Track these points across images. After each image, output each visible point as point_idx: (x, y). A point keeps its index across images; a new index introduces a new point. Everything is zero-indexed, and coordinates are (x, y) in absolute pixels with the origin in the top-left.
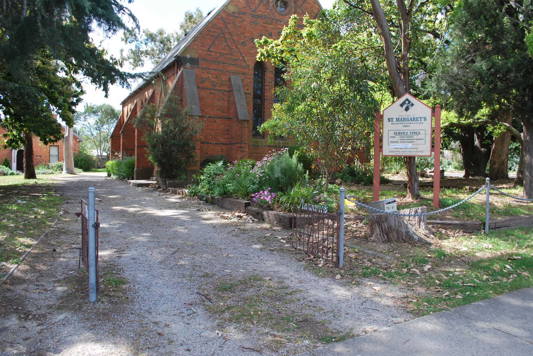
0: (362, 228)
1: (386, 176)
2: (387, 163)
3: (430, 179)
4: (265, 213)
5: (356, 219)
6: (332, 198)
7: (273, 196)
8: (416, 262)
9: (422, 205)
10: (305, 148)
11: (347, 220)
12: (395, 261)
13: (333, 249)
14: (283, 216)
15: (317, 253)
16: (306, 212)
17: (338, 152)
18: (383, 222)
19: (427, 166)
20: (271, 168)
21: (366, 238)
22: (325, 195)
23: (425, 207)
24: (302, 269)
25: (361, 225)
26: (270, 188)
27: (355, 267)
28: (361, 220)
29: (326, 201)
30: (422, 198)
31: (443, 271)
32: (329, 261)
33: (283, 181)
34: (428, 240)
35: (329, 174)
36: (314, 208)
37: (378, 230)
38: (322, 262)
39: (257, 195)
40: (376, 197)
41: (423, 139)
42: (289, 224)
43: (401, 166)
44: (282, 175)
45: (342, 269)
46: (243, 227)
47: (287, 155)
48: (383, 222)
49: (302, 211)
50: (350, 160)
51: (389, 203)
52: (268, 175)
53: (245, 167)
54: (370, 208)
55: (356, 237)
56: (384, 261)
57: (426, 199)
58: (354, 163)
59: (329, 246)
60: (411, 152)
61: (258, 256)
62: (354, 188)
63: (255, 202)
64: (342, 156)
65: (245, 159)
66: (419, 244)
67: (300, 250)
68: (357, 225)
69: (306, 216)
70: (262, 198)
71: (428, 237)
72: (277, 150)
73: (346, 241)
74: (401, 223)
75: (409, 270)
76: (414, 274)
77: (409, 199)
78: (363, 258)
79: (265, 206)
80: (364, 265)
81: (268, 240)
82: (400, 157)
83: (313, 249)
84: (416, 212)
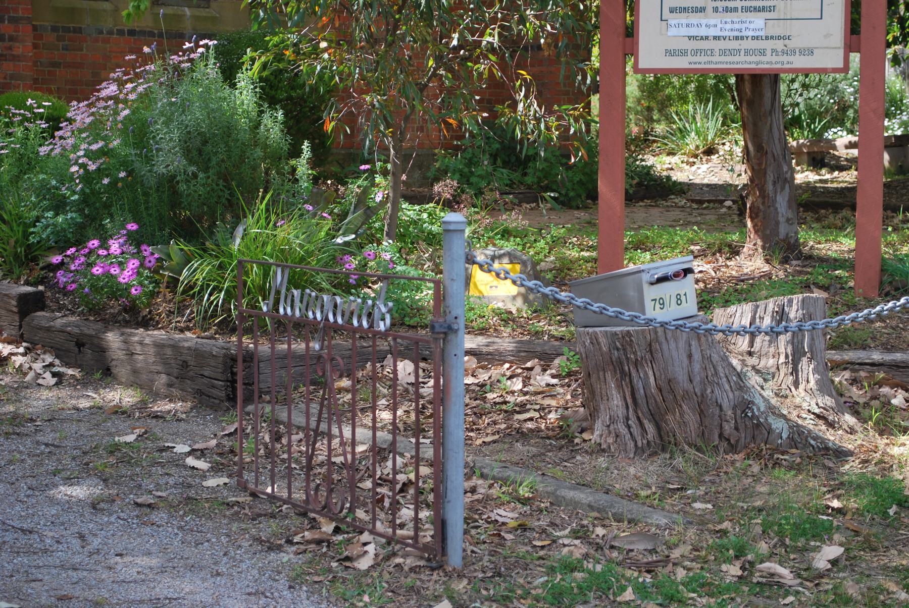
0: (548, 392)
1: (660, 163)
2: (663, 105)
3: (848, 177)
4: (113, 338)
5: (523, 354)
6: (418, 265)
7: (151, 262)
8: (781, 534)
9: (807, 287)
10: (294, 38)
11: (484, 358)
12: (691, 533)
13: (419, 492)
14: (198, 354)
15: (351, 510)
16: (302, 328)
17: (439, 59)
18: (636, 364)
19: (838, 121)
20: (139, 133)
21: (564, 437)
22: (387, 250)
23: (818, 294)
24: (283, 583)
25: (542, 379)
26: (132, 227)
27: (516, 565)
28: (546, 360)
29: (387, 278)
30: (810, 259)
31: (896, 569)
32: (402, 541)
33: (198, 187)
34: (831, 436)
35: (405, 158)
36: (326, 308)
37: (616, 401)
38: (371, 548)
39: (73, 258)
40: (610, 256)
41: (672, 10)
42: (226, 385)
43: (727, 120)
44: (191, 162)
45: (461, 576)
46: (11, 408)
47: (212, 70)
48: (636, 364)
49: (284, 327)
50: (498, 94)
51: (663, 279)
52: (125, 164)
53: (19, 132)
54: (580, 301)
55: (523, 435)
56: (644, 535)
57: (824, 261)
58: (515, 104)
59: (401, 478)
60: (763, 52)
61: (82, 537)
62: (514, 219)
63: (65, 292)
64: (462, 76)
65: (15, 94)
66: (794, 456)
67: (272, 498)
68: (526, 381)
69: (299, 346)
70: (97, 270)
71: (831, 425)
72: (161, 51)
73: (478, 452)
74: (714, 367)
75: (748, 567)
76: (772, 584)
77: (752, 262)
78: (553, 524)
79: (115, 307)
80: (555, 554)
81: (126, 461)
82: (721, 76)
83: (331, 491)
84: (781, 315)
